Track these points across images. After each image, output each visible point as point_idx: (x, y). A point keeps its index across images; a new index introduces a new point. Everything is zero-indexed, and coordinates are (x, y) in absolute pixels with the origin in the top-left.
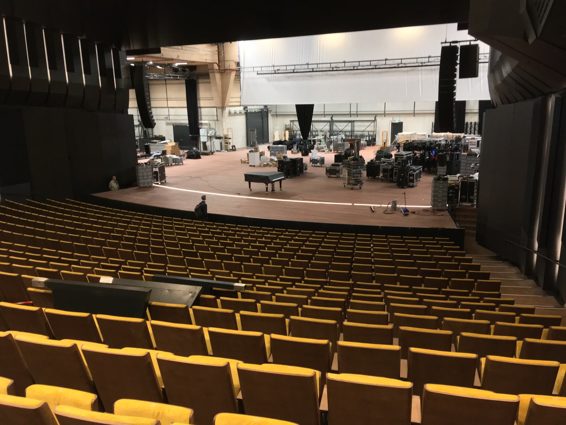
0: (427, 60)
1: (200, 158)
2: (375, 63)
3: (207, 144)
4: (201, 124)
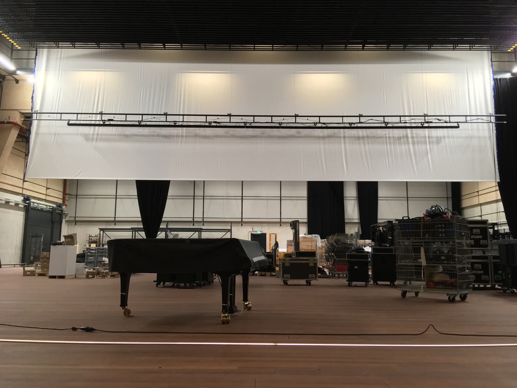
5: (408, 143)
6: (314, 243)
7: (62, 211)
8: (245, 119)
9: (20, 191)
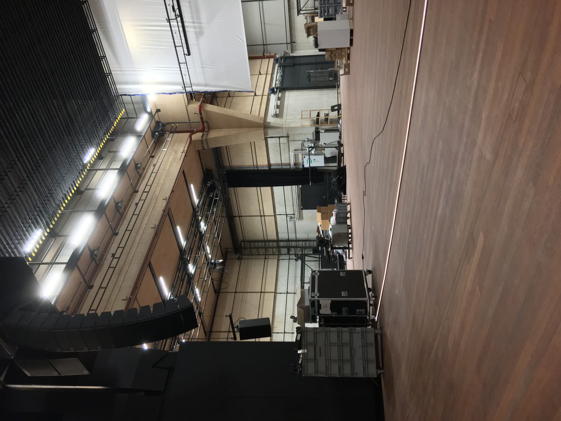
1: (345, 167)
3: (328, 155)
4: (295, 164)
7: (281, 58)
9: (265, 98)
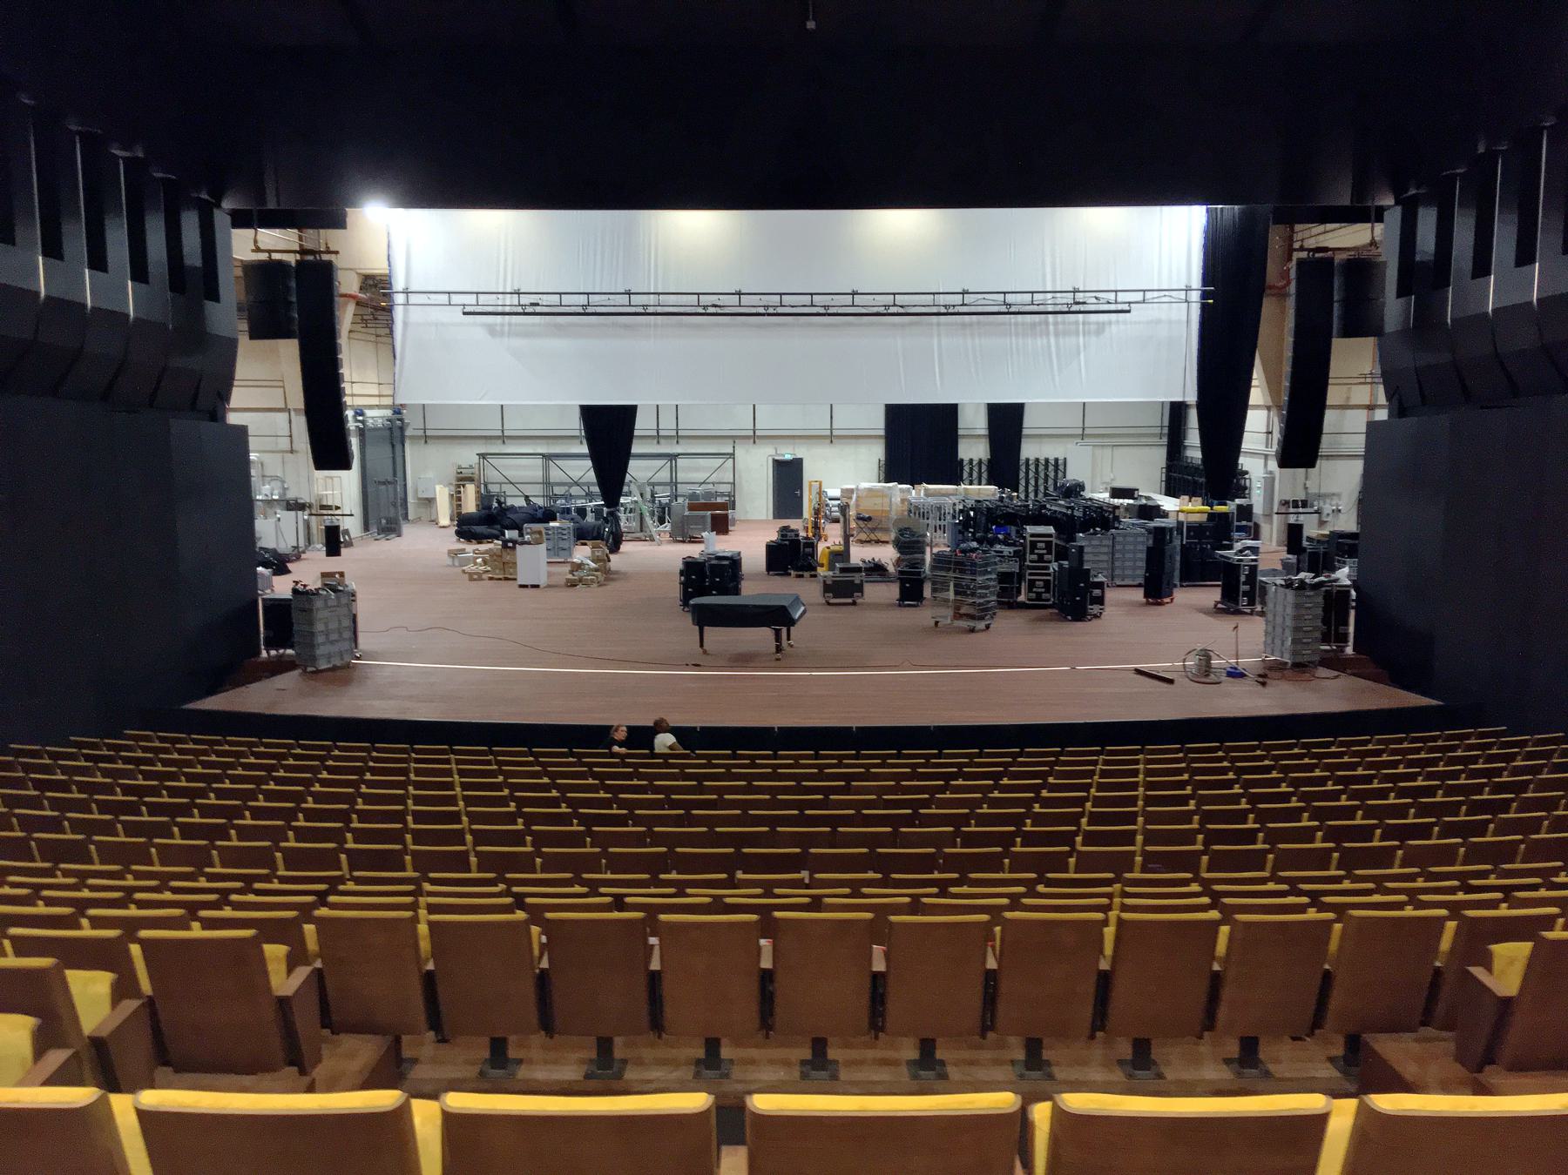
0: (848, 300)
2: (826, 300)
5: (1048, 334)
6: (886, 500)
8: (766, 300)
